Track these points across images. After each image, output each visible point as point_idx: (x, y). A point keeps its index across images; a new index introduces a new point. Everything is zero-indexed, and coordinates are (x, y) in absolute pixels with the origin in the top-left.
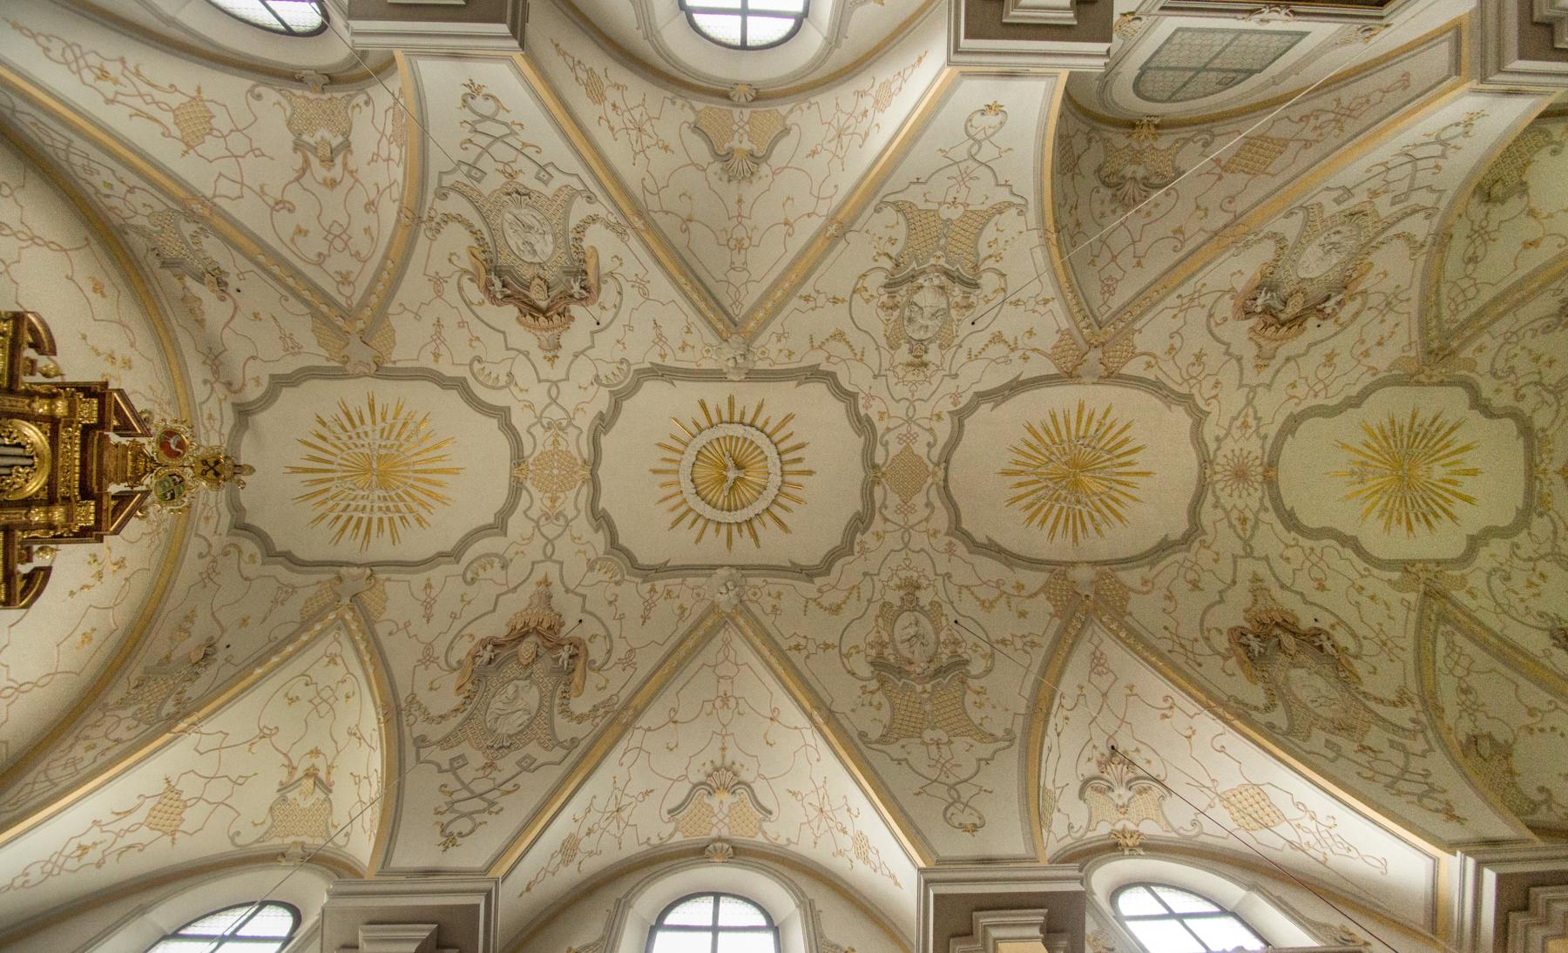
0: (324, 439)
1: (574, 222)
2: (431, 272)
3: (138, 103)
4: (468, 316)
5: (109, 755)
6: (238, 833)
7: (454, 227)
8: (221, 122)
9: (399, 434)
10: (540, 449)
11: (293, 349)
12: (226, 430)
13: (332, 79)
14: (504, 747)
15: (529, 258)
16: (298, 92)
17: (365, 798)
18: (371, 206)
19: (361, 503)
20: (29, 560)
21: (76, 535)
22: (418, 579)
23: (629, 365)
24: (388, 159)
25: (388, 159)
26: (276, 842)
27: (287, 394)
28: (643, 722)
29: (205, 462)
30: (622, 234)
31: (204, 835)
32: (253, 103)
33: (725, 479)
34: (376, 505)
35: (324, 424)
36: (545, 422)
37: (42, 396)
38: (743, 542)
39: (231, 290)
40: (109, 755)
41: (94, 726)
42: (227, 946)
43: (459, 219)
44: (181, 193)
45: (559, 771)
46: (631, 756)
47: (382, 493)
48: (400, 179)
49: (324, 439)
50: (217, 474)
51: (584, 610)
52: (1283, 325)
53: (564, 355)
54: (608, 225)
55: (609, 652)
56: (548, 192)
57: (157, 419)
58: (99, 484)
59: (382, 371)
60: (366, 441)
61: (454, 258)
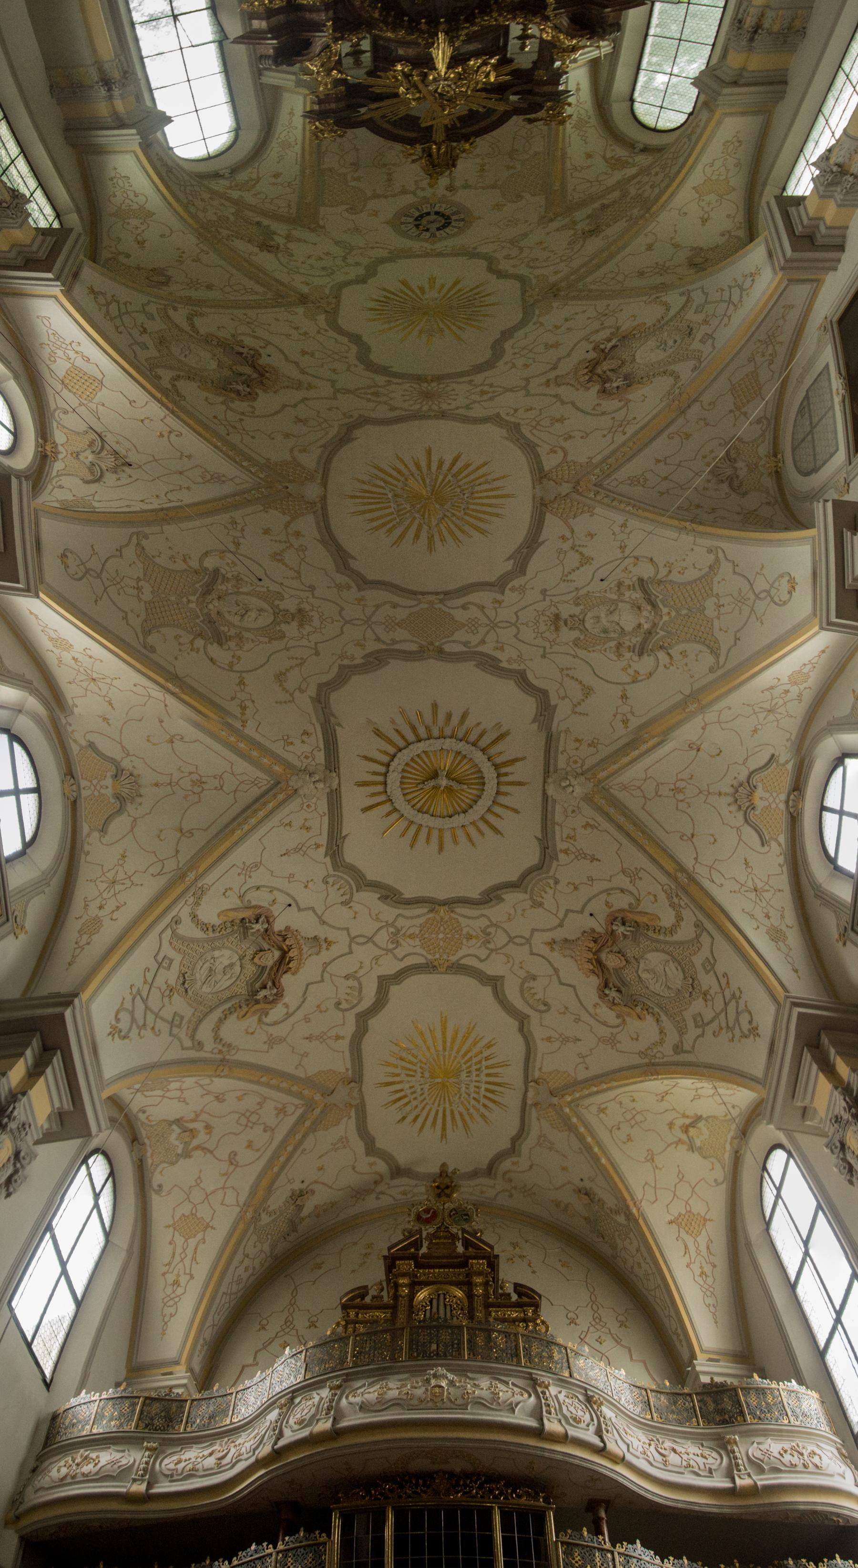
0: (417, 1117)
1: (198, 934)
2: (266, 1047)
3: (187, 1261)
4: (300, 1015)
5: (645, 1254)
6: (716, 1181)
7: (224, 1033)
8: (186, 1209)
9: (410, 1062)
10: (419, 950)
11: (344, 1142)
12: (413, 1182)
13: (134, 1139)
14: (692, 984)
15: (237, 969)
16: (150, 1161)
17: (712, 1092)
18: (220, 1098)
19: (472, 1089)
20: (509, 1294)
21: (493, 1270)
22: (542, 1047)
23: (328, 876)
24: (181, 1090)
25: (181, 1090)
26: (727, 1156)
27: (380, 1144)
28: (689, 863)
29: (439, 1195)
30: (203, 891)
31: (711, 1203)
32: (166, 1189)
33: (449, 789)
34: (474, 1078)
35: (404, 1118)
36: (391, 946)
37: (396, 1290)
38: (518, 772)
39: (304, 1186)
40: (645, 1254)
41: (625, 1263)
42: (783, 1193)
43: (217, 1029)
44: (241, 1226)
45: (719, 938)
46: (718, 879)
47: (464, 1075)
48: (193, 1079)
49: (417, 1117)
50: (447, 1187)
51: (582, 912)
52: (262, 375)
53: (322, 932)
54: (197, 904)
55: (622, 891)
56: (178, 958)
57: (409, 1227)
58: (456, 1257)
59: (356, 1078)
60: (418, 1088)
61: (251, 1030)
